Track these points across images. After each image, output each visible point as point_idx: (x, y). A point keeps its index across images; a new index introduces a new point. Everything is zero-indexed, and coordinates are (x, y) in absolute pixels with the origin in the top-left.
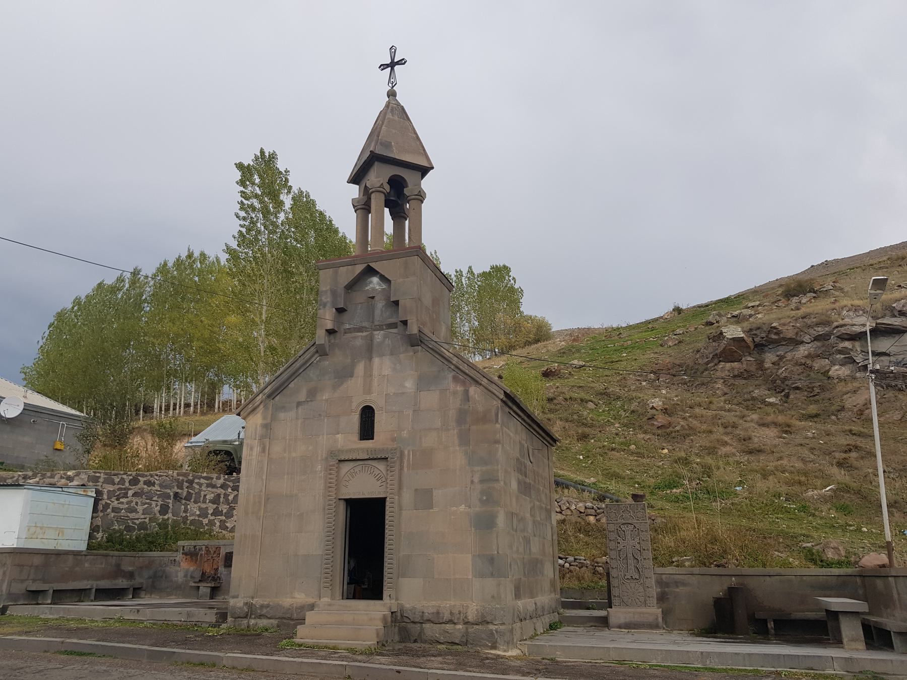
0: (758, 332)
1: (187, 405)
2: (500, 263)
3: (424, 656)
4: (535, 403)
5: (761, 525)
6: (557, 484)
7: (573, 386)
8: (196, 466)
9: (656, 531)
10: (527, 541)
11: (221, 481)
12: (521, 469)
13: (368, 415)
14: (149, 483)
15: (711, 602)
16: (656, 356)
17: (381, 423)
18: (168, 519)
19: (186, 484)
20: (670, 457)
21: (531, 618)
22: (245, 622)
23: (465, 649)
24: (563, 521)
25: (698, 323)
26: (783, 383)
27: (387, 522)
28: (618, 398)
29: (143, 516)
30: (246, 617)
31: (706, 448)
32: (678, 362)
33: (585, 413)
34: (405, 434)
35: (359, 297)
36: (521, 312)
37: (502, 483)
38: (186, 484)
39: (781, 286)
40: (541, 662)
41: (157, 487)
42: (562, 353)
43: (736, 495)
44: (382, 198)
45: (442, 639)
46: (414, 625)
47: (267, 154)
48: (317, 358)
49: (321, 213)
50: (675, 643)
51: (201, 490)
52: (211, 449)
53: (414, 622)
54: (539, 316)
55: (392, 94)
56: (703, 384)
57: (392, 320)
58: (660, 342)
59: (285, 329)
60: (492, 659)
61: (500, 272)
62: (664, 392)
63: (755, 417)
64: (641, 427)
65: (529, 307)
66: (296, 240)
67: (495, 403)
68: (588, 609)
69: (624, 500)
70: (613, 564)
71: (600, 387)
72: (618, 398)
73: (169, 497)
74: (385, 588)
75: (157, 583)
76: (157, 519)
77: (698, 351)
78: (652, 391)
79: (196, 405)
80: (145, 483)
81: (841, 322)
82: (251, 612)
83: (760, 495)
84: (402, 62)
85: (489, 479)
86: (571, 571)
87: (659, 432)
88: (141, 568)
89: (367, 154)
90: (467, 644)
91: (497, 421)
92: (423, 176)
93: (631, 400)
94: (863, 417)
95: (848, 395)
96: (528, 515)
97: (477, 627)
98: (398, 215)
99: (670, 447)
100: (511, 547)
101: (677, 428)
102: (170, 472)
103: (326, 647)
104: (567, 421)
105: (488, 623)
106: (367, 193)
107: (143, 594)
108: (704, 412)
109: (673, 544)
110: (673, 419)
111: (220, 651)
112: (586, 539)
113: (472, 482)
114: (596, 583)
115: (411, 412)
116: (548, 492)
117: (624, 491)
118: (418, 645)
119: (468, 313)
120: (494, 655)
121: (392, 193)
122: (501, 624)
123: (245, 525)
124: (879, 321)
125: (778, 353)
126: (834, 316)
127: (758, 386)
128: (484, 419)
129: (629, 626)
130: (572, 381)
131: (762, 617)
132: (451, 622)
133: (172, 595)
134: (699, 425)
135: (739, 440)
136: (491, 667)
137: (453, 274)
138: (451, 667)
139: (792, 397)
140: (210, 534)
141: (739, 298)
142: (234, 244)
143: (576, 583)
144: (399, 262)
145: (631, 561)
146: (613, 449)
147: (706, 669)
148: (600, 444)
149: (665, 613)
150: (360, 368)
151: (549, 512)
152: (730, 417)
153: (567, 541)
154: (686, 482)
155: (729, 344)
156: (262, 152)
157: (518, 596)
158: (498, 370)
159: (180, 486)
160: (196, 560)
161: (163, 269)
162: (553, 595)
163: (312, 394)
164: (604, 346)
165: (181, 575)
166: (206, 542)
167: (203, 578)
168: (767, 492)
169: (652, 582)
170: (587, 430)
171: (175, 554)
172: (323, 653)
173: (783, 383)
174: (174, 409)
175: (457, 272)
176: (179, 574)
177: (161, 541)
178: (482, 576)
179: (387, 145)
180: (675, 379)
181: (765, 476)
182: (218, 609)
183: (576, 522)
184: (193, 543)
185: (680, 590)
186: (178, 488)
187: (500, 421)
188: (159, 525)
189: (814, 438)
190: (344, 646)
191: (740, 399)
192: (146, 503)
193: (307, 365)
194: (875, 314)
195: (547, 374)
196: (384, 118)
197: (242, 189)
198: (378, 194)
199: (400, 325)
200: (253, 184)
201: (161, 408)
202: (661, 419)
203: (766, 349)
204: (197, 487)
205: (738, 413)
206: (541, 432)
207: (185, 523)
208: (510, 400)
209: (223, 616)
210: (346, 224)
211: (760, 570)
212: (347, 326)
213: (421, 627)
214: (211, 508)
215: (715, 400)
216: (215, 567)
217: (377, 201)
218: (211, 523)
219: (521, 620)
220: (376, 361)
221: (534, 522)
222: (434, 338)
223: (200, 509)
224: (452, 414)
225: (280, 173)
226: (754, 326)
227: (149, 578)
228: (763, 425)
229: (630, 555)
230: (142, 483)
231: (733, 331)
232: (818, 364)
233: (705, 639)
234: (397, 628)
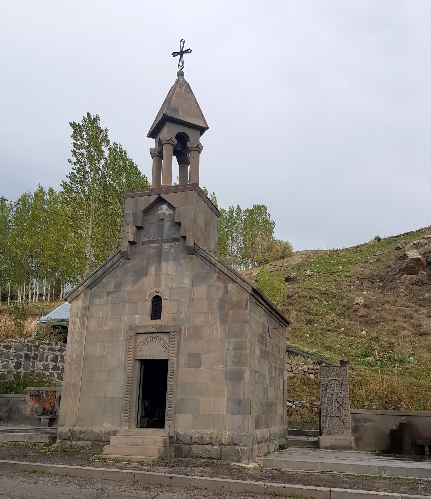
1: (41, 295)
2: (260, 203)
3: (191, 467)
4: (278, 298)
5: (424, 383)
6: (288, 352)
8: (41, 336)
10: (265, 390)
11: (59, 346)
12: (263, 341)
13: (157, 302)
15: (388, 432)
16: (362, 269)
17: (167, 308)
18: (21, 372)
19: (33, 348)
20: (367, 336)
21: (266, 441)
22: (69, 442)
23: (220, 462)
24: (293, 377)
25: (391, 248)
28: (335, 297)
30: (69, 439)
31: (391, 331)
32: (375, 273)
33: (312, 306)
34: (183, 315)
35: (153, 219)
36: (273, 238)
37: (248, 351)
38: (33, 348)
40: (270, 472)
43: (409, 362)
44: (171, 148)
45: (204, 455)
47: (92, 117)
48: (122, 261)
49: (130, 161)
50: (362, 459)
51: (44, 353)
54: (285, 241)
55: (180, 74)
56: (391, 289)
58: (365, 260)
61: (260, 210)
62: (365, 293)
63: (425, 311)
64: (348, 316)
65: (278, 234)
66: (113, 180)
67: (246, 295)
68: (307, 435)
70: (324, 406)
71: (322, 289)
72: (335, 297)
73: (21, 357)
74: (166, 421)
76: (13, 372)
77: (389, 267)
79: (47, 295)
82: (73, 436)
83: (425, 363)
84: (188, 51)
85: (239, 347)
86: (296, 411)
87: (361, 320)
89: (161, 116)
90: (221, 460)
91: (246, 308)
92: (201, 134)
93: (343, 298)
96: (267, 373)
97: (228, 447)
99: (368, 330)
100: (253, 393)
101: (373, 318)
102: (22, 340)
104: (300, 311)
105: (236, 445)
106: (160, 144)
108: (391, 307)
110: (370, 312)
111: (48, 463)
113: (228, 349)
114: (313, 418)
115: (187, 301)
116: (282, 357)
118: (188, 459)
120: (239, 466)
121: (179, 145)
122: (245, 446)
123: (70, 377)
128: (237, 306)
129: (333, 448)
130: (304, 284)
131: (421, 444)
132: (210, 444)
134: (387, 316)
135: (414, 326)
136: (235, 475)
138: (208, 474)
140: (49, 383)
142: (68, 181)
143: (300, 418)
144: (180, 195)
145: (336, 404)
146: (329, 331)
147: (381, 478)
148: (321, 327)
149: (357, 440)
150: (152, 269)
151: (282, 371)
152: (408, 311)
154: (376, 353)
155: (410, 262)
156: (89, 115)
157: (257, 426)
158: (255, 276)
159: (29, 350)
160: (40, 400)
161: (24, 199)
162: (282, 426)
163: (118, 286)
164: (327, 262)
165: (28, 410)
166: (46, 388)
167: (45, 412)
169: (350, 419)
170: (313, 317)
171: (25, 396)
175: (230, 208)
177: (15, 387)
178: (232, 412)
179: (176, 110)
180: (373, 285)
182: (51, 433)
184: (37, 388)
185: (368, 424)
187: (248, 308)
188: (14, 376)
190: (135, 460)
191: (415, 299)
192: (5, 361)
193: (114, 266)
195: (288, 280)
198: (168, 145)
199: (182, 241)
200: (82, 138)
202: (362, 311)
204: (42, 350)
205: (414, 309)
207: (32, 375)
208: (256, 294)
209: (53, 439)
210: (146, 167)
212: (144, 239)
213: (191, 448)
215: (399, 299)
216: (52, 405)
217: (167, 150)
218: (52, 375)
220: (164, 264)
221: (271, 377)
223: (43, 365)
224: (216, 302)
225: (102, 131)
226: (428, 250)
227: (6, 412)
229: (335, 401)
231: (413, 254)
233: (382, 457)
234: (173, 448)
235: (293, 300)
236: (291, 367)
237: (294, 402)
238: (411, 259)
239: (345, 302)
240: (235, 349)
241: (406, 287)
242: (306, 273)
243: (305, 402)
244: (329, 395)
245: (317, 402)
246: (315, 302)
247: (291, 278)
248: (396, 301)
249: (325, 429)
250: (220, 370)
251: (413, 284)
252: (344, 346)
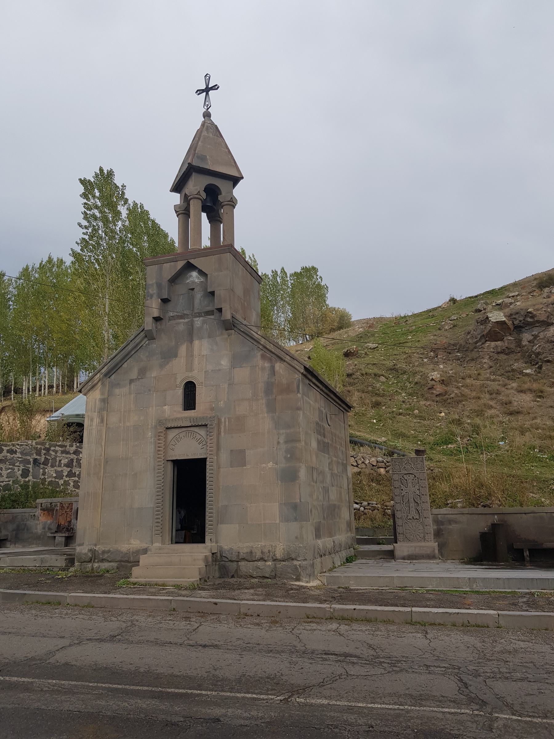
0: (517, 316)
2: (309, 265)
3: (239, 589)
4: (337, 377)
5: (519, 472)
7: (368, 364)
8: (52, 436)
9: (434, 479)
10: (326, 490)
11: (74, 448)
12: (320, 431)
13: (190, 389)
14: (12, 452)
16: (435, 337)
17: (202, 396)
18: (29, 481)
22: (90, 565)
23: (274, 581)
24: (359, 473)
26: (537, 357)
27: (207, 478)
29: (7, 480)
30: (90, 562)
31: (475, 411)
32: (452, 342)
33: (378, 385)
35: (181, 289)
36: (327, 305)
37: (303, 443)
39: (536, 279)
40: (336, 591)
41: (18, 455)
42: (360, 338)
43: (499, 448)
44: (199, 204)
46: (230, 563)
47: (105, 172)
48: (146, 342)
50: (448, 570)
52: (64, 422)
53: (231, 561)
55: (207, 115)
56: (473, 360)
57: (209, 308)
58: (439, 326)
59: (125, 320)
60: (297, 589)
62: (441, 366)
63: (515, 385)
64: (423, 395)
65: (333, 301)
68: (379, 544)
69: (409, 454)
70: (398, 507)
72: (405, 372)
73: (29, 463)
74: (206, 534)
75: (20, 534)
78: (432, 366)
79: (58, 386)
80: (8, 451)
82: (94, 557)
83: (519, 448)
84: (216, 87)
85: (292, 440)
86: (365, 514)
87: (438, 399)
88: (6, 522)
90: (276, 579)
91: (298, 392)
92: (235, 185)
93: (415, 373)
96: (327, 469)
97: (284, 563)
98: (214, 219)
101: (452, 396)
102: (30, 442)
103: (156, 585)
105: (293, 559)
106: (186, 199)
107: (8, 544)
108: (474, 382)
109: (447, 490)
111: (65, 591)
114: (386, 522)
115: (226, 386)
116: (344, 450)
117: (409, 447)
118: (235, 580)
119: (283, 306)
120: (298, 586)
121: (208, 199)
123: (89, 485)
125: (533, 333)
127: (517, 360)
128: (287, 389)
129: (411, 557)
130: (369, 359)
132: (262, 559)
133: (33, 544)
134: (470, 393)
135: (502, 404)
137: (270, 274)
138: (261, 598)
139: (544, 368)
140: (64, 492)
141: (503, 290)
142: (78, 249)
143: (370, 523)
144: (214, 258)
145: (412, 504)
146: (400, 414)
147: (473, 592)
149: (441, 547)
150: (183, 350)
151: (345, 466)
152: (494, 386)
153: (362, 490)
154: (459, 439)
155: (493, 327)
156: (101, 170)
157: (318, 536)
159: (39, 454)
160: (53, 515)
161: (25, 273)
162: (349, 534)
163: (143, 372)
164: (392, 331)
166: (60, 500)
167: (59, 529)
168: (524, 445)
169: (430, 521)
170: (379, 399)
171: (34, 510)
172: (153, 590)
173: (537, 357)
174: (40, 390)
175: (273, 272)
176: (38, 527)
178: (286, 520)
179: (203, 158)
180: (450, 356)
181: (522, 433)
183: (370, 474)
184: (49, 500)
185: (452, 527)
186: (37, 455)
188: (21, 486)
190: (171, 583)
191: (502, 371)
192: (10, 469)
193: (137, 348)
195: (347, 355)
196: (200, 135)
197: (85, 201)
198: (195, 200)
199: (217, 314)
200: (94, 197)
201: (28, 389)
202: (439, 389)
203: (523, 330)
204: (54, 454)
205: (501, 383)
206: (337, 400)
207: (43, 484)
208: (310, 374)
209: (71, 561)
210: (170, 225)
211: (517, 509)
212: (171, 314)
213: (237, 565)
214: (66, 471)
215: (482, 372)
216: (69, 519)
217: (195, 206)
218: (66, 483)
219: (321, 556)
220: (196, 343)
222: (245, 322)
223: (56, 472)
224: (261, 386)
226: (514, 311)
228: (521, 391)
229: (412, 500)
230: (5, 451)
231: (497, 316)
233: (473, 566)
234: (217, 566)
235: (354, 379)
236: (356, 461)
237: (361, 503)
238: (495, 322)
239: (417, 378)
240: (286, 442)
241: (490, 357)
243: (375, 503)
244: (404, 493)
247: (350, 352)
248: (479, 374)
250: (269, 468)
251: (498, 353)
252: (420, 432)
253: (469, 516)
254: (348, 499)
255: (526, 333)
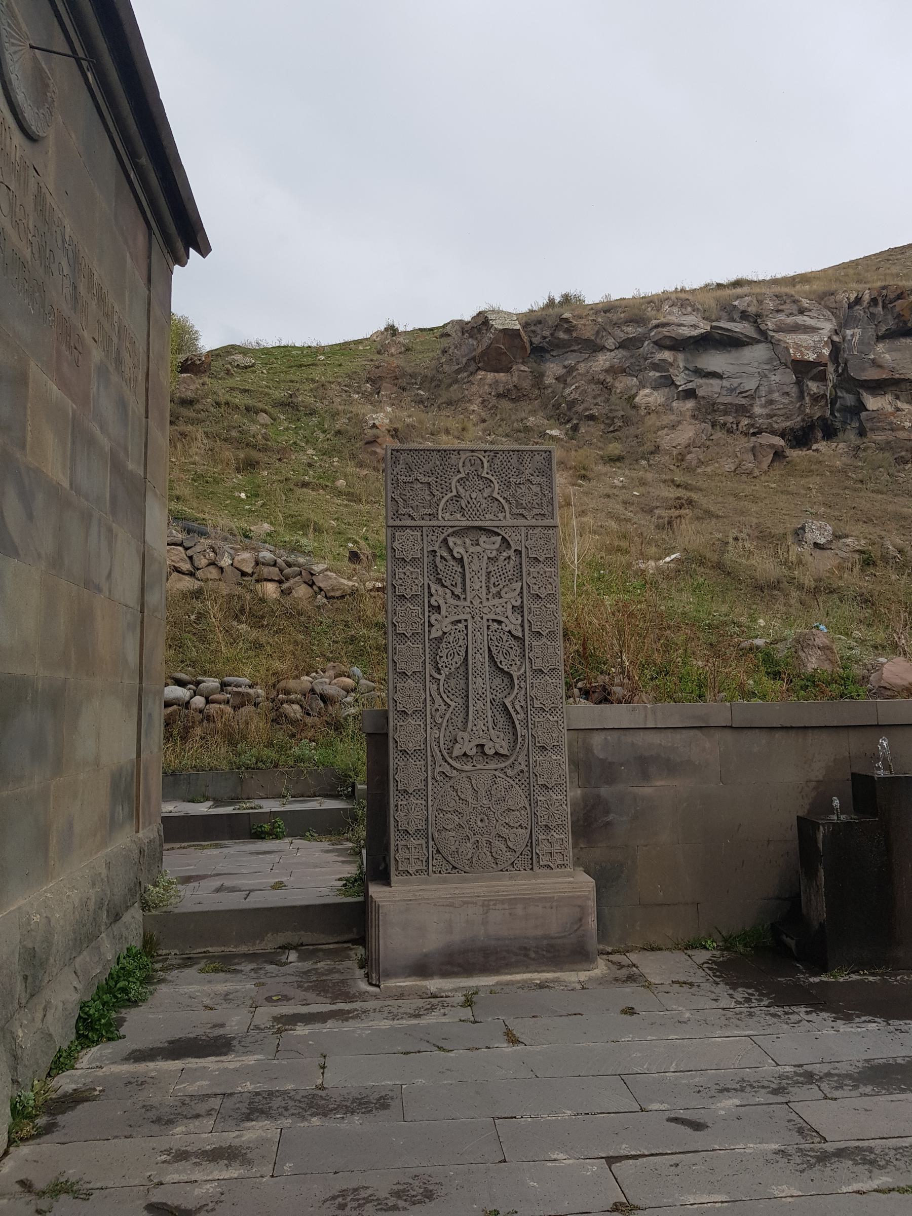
24: (197, 594)
28: (312, 413)
56: (449, 403)
64: (353, 456)
71: (279, 394)
72: (312, 413)
81: (663, 320)
86: (208, 718)
94: (685, 464)
95: (665, 431)
112: (254, 634)
114: (283, 749)
124: (714, 324)
125: (566, 363)
126: (650, 312)
127: (533, 412)
130: (236, 381)
139: (582, 430)
145: (482, 682)
146: (305, 485)
149: (605, 879)
153: (203, 640)
155: (496, 340)
169: (557, 765)
170: (255, 455)
173: (569, 409)
183: (231, 597)
185: (657, 789)
189: (623, 487)
194: (707, 314)
203: (548, 356)
232: (623, 383)
235: (198, 412)
236: (191, 558)
237: (198, 683)
241: (484, 401)
242: (234, 360)
243: (246, 681)
244: (442, 624)
245: (297, 677)
246: (262, 421)
247: (193, 363)
248: (463, 429)
249: (413, 842)
251: (499, 396)
252: (349, 524)
253: (728, 736)
254: (132, 657)
255: (552, 362)
